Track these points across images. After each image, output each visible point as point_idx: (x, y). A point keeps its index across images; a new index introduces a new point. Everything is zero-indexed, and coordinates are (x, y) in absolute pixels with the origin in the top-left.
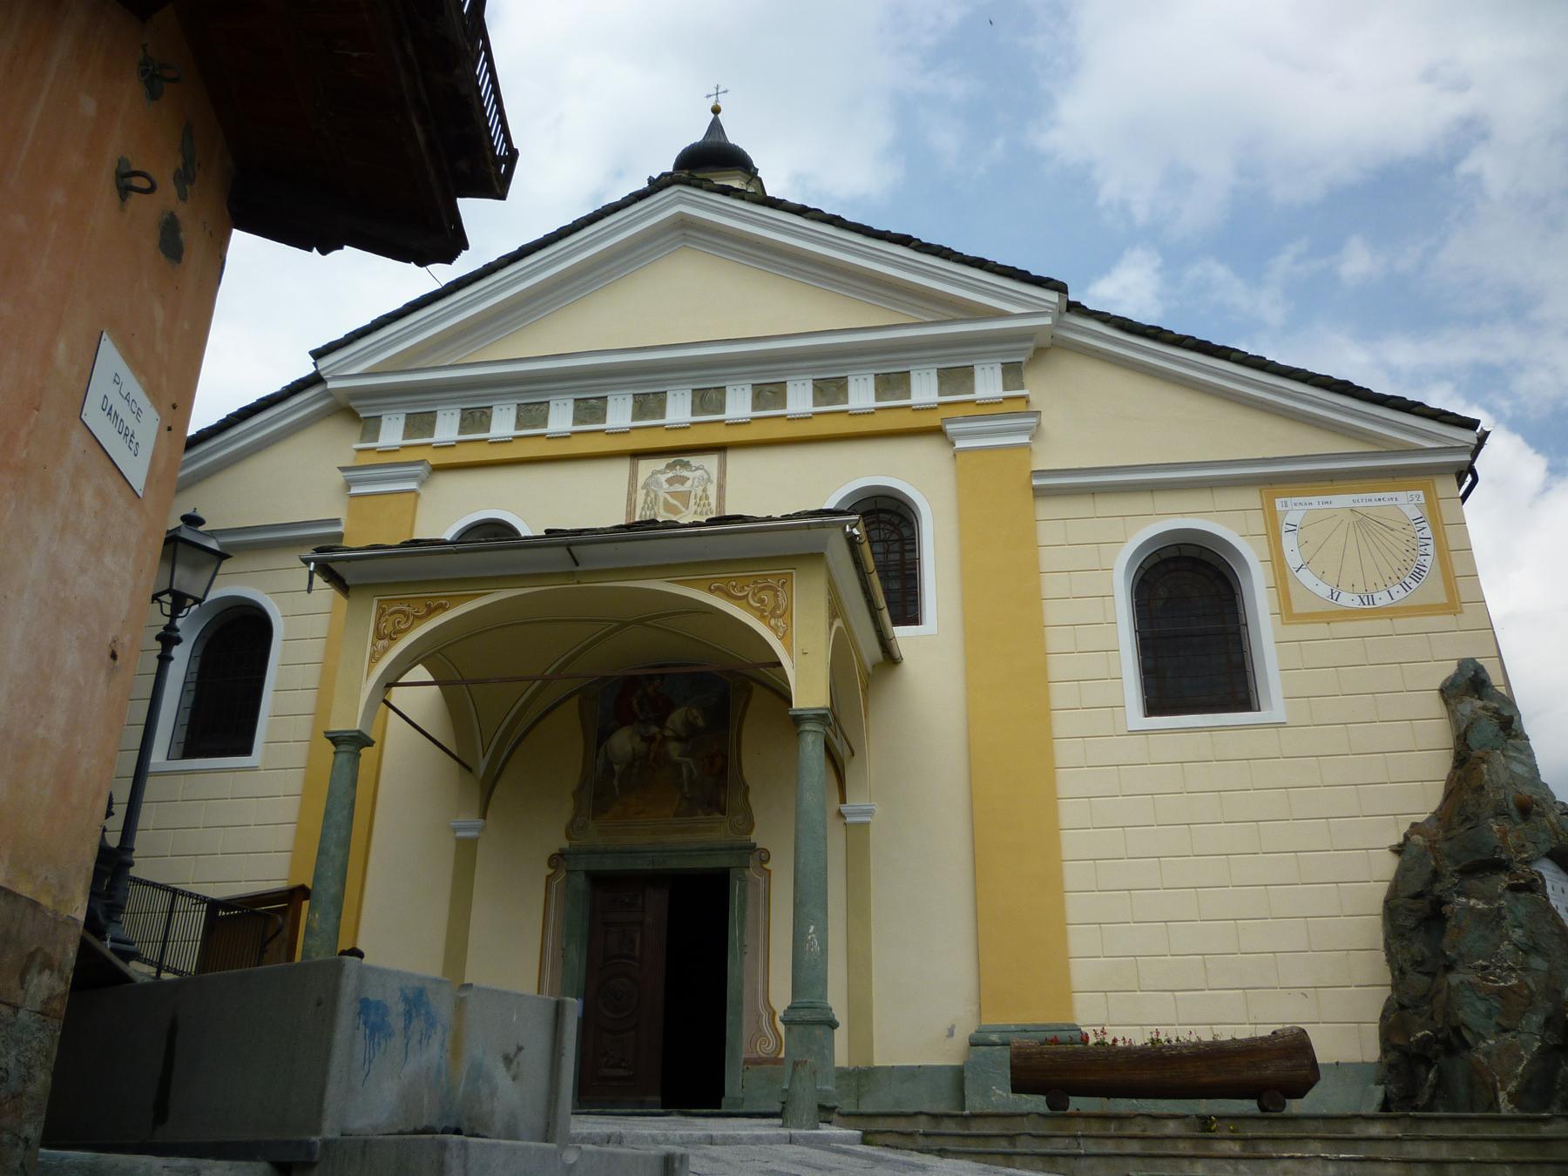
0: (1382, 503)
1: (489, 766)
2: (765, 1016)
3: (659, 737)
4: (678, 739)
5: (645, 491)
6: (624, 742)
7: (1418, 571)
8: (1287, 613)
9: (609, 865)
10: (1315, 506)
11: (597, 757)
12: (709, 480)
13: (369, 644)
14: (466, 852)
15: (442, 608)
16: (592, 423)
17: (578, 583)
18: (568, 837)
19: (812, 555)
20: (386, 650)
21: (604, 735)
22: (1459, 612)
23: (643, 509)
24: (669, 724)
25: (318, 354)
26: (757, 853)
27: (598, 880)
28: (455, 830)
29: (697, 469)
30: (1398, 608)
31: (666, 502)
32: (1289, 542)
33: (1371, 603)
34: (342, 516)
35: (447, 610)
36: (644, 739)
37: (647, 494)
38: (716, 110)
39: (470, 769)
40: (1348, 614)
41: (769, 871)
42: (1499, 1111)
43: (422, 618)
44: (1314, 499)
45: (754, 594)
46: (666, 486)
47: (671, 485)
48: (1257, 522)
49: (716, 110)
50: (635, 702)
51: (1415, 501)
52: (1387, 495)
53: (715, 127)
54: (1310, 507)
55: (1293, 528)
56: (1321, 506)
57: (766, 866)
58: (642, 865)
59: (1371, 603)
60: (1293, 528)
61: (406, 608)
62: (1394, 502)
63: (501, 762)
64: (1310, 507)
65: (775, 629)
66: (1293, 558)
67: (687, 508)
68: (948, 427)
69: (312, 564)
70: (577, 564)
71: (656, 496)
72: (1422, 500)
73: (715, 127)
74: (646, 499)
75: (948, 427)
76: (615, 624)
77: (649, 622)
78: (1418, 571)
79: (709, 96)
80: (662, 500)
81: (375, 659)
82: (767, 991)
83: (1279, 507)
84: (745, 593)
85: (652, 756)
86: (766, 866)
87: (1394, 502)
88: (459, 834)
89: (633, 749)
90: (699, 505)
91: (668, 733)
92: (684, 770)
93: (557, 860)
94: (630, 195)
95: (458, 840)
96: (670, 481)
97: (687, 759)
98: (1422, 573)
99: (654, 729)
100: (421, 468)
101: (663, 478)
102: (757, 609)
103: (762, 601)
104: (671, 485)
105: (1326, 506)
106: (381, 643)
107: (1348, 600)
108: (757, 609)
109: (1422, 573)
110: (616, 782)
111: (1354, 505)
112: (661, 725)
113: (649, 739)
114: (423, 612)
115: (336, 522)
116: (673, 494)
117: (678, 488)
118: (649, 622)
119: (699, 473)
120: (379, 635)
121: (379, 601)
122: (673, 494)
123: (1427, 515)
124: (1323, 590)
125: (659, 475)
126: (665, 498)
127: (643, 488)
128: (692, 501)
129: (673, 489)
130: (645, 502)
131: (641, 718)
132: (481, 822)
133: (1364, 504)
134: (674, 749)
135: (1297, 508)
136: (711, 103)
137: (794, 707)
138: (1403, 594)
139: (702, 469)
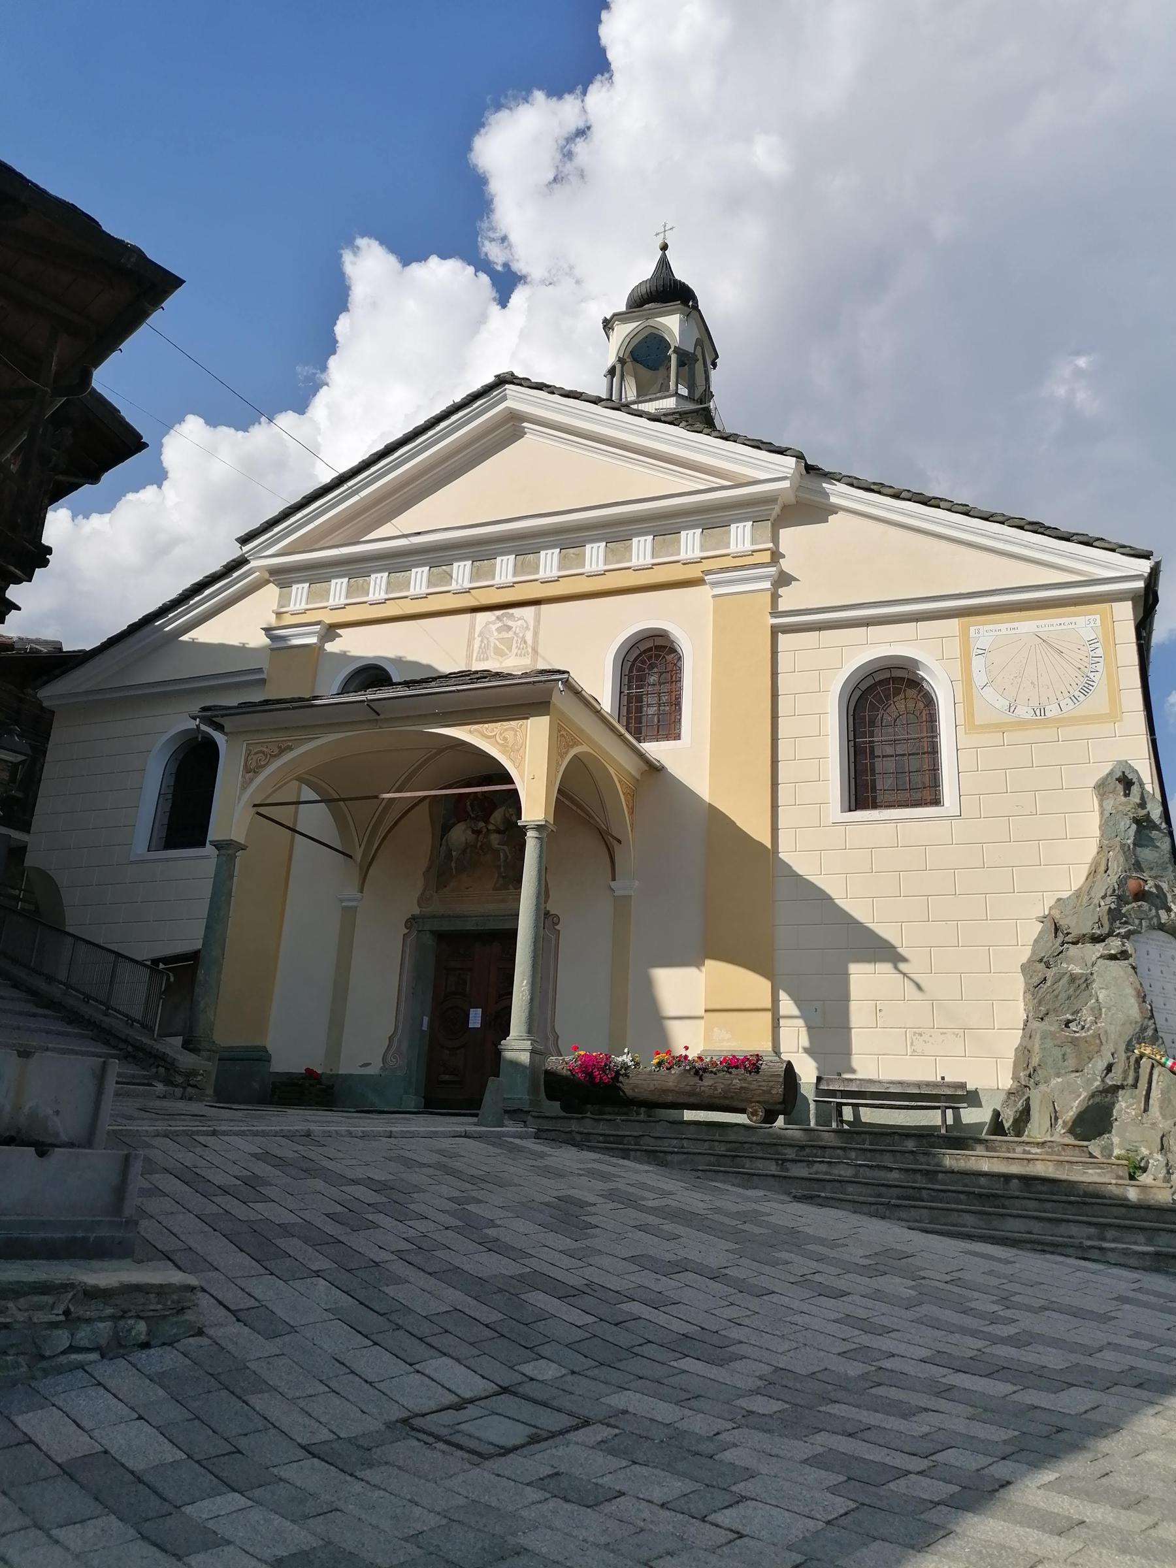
0: (1063, 627)
1: (364, 854)
2: (551, 1039)
3: (484, 830)
4: (498, 832)
5: (480, 639)
6: (460, 834)
7: (1086, 685)
8: (972, 726)
9: (446, 926)
10: (1004, 632)
11: (441, 846)
12: (527, 628)
13: (240, 776)
14: (349, 915)
15: (290, 748)
16: (442, 586)
17: (381, 728)
18: (420, 906)
19: (542, 703)
20: (251, 780)
21: (446, 829)
22: (1118, 721)
23: (479, 652)
24: (492, 820)
25: (244, 540)
26: (551, 918)
27: (440, 936)
28: (342, 901)
29: (519, 619)
30: (1064, 718)
31: (496, 647)
32: (977, 663)
33: (1043, 714)
34: (266, 666)
35: (292, 750)
36: (474, 832)
37: (482, 641)
38: (664, 247)
39: (350, 857)
40: (1022, 725)
41: (559, 931)
42: (809, 1125)
43: (276, 756)
44: (1003, 626)
45: (501, 734)
46: (496, 634)
47: (499, 633)
48: (954, 648)
49: (664, 247)
50: (468, 803)
51: (1092, 625)
52: (1067, 620)
53: (664, 264)
54: (1000, 633)
55: (982, 652)
56: (1009, 632)
57: (556, 927)
58: (470, 926)
59: (1043, 714)
60: (982, 652)
61: (265, 749)
62: (1073, 626)
63: (373, 852)
64: (1000, 633)
65: (513, 762)
66: (979, 678)
67: (510, 651)
68: (706, 578)
69: (198, 720)
70: (378, 714)
71: (488, 642)
72: (1098, 623)
73: (664, 264)
74: (481, 645)
75: (706, 578)
76: (434, 751)
77: (459, 748)
78: (1086, 685)
79: (657, 234)
80: (492, 645)
81: (244, 788)
82: (553, 1021)
83: (972, 634)
84: (494, 734)
85: (479, 844)
86: (556, 927)
87: (1073, 626)
88: (344, 904)
89: (466, 839)
90: (519, 649)
91: (491, 827)
92: (501, 854)
93: (412, 921)
94: (468, 396)
95: (344, 908)
96: (499, 630)
97: (505, 847)
98: (1090, 688)
99: (481, 824)
100: (319, 626)
101: (494, 627)
102: (502, 745)
103: (505, 739)
104: (499, 633)
105: (1014, 632)
106: (248, 775)
107: (1024, 712)
108: (502, 745)
109: (1090, 688)
110: (453, 865)
111: (1037, 630)
112: (487, 822)
113: (477, 832)
114: (276, 751)
115: (260, 670)
116: (501, 640)
117: (505, 635)
118: (459, 748)
119: (520, 622)
120: (247, 770)
121: (247, 744)
122: (501, 640)
123: (1101, 637)
124: (1002, 704)
125: (491, 625)
126: (495, 644)
127: (479, 636)
128: (514, 645)
129: (501, 636)
130: (480, 647)
131: (472, 816)
132: (359, 895)
133: (1046, 629)
134: (495, 839)
135: (987, 634)
136: (659, 242)
137: (523, 819)
138: (1071, 706)
139: (523, 619)
